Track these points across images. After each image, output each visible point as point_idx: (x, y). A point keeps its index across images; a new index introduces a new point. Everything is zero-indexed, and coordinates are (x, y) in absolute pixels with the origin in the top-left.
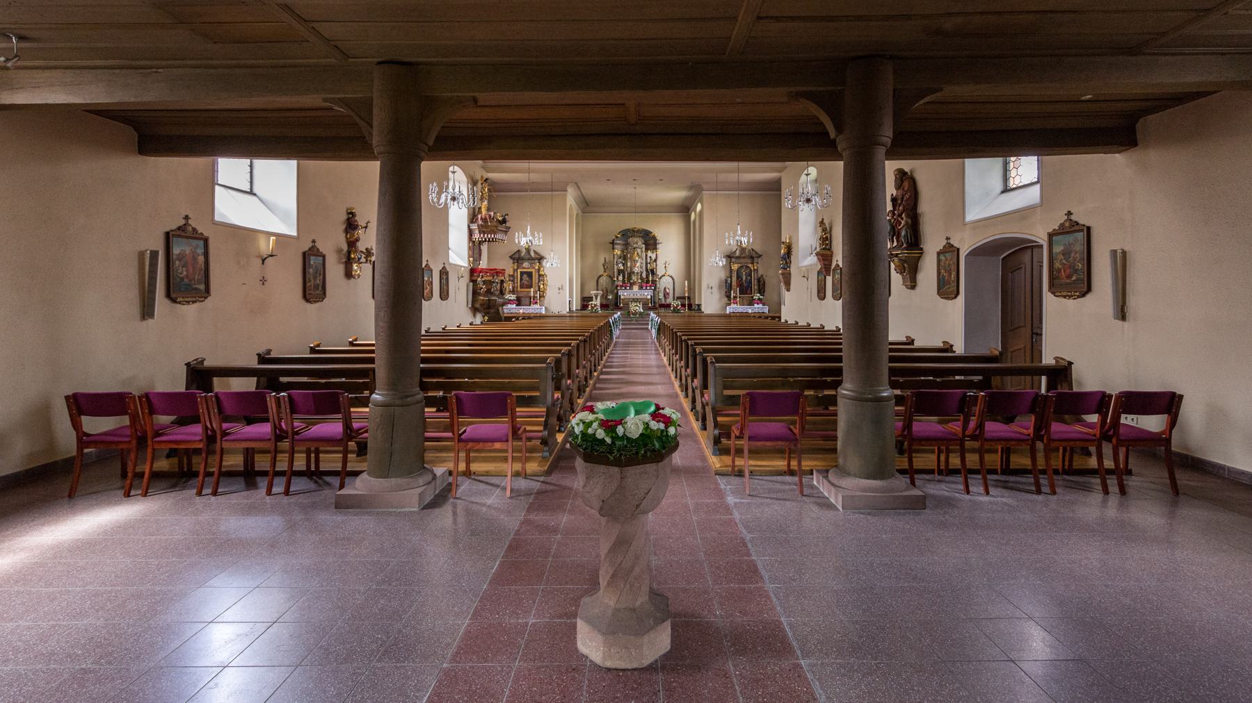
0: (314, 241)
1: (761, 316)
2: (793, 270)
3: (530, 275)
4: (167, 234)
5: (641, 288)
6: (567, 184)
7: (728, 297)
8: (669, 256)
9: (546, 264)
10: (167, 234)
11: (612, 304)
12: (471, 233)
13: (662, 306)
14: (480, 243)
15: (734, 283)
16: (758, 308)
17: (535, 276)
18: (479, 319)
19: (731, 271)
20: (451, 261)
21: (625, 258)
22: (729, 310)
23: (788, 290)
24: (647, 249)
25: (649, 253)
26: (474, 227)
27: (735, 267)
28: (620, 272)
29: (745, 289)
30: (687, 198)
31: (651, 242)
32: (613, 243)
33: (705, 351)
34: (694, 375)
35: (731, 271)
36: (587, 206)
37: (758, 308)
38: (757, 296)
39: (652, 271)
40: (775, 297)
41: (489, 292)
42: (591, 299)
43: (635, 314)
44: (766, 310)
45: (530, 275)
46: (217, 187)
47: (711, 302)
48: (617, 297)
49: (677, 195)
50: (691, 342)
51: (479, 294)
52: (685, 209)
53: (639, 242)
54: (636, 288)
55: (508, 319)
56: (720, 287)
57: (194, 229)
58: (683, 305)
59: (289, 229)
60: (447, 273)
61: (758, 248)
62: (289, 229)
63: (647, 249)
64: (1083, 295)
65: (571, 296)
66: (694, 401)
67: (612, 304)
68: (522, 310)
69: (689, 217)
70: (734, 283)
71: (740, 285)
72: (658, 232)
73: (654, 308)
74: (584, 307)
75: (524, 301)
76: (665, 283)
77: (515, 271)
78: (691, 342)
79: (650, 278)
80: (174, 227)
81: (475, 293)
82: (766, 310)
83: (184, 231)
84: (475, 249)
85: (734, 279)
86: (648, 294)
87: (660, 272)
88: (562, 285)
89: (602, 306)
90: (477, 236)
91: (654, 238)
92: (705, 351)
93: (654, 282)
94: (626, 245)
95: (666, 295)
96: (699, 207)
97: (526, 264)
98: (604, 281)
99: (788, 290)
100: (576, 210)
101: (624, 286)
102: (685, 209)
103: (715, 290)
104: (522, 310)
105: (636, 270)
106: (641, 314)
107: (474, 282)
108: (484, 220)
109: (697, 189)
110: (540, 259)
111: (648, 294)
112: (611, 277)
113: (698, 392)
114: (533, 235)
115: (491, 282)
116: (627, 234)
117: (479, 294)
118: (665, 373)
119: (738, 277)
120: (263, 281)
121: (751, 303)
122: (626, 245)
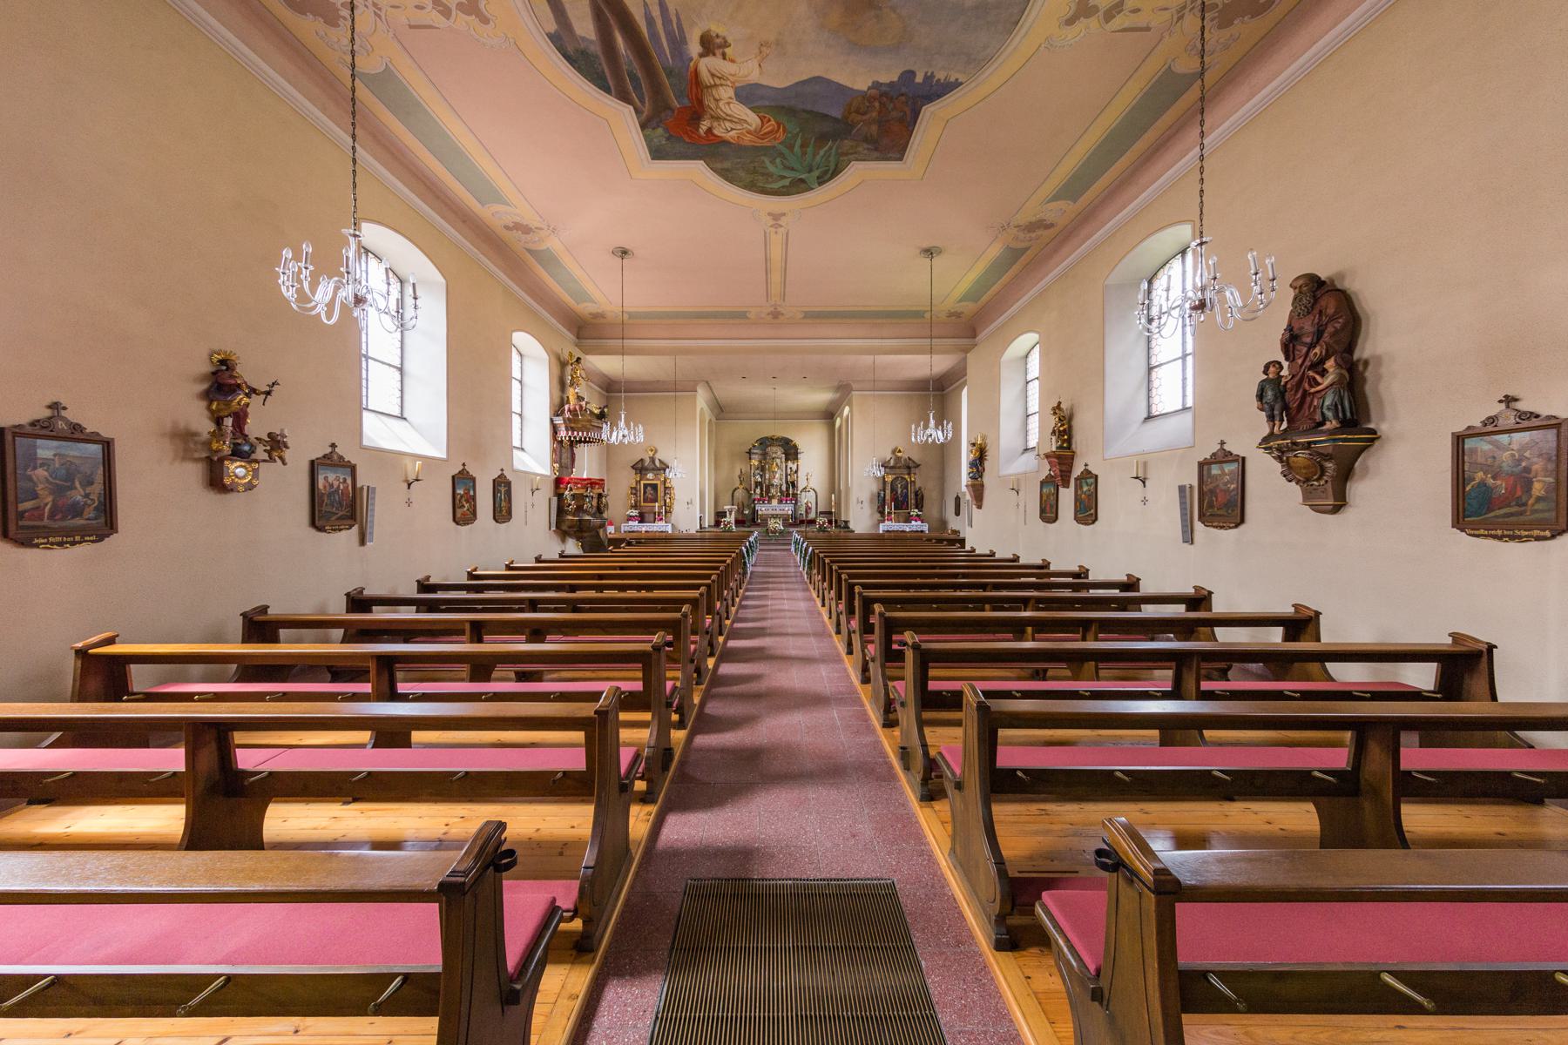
0: (333, 446)
1: (918, 536)
2: (987, 479)
3: (655, 487)
4: (312, 462)
5: (780, 502)
6: (696, 383)
7: (882, 513)
8: (811, 469)
9: (670, 474)
10: (312, 462)
11: (749, 519)
12: (555, 429)
13: (802, 522)
14: (572, 443)
15: (888, 497)
16: (915, 525)
17: (661, 489)
18: (572, 547)
19: (884, 482)
20: (517, 465)
21: (763, 469)
22: (882, 528)
23: (979, 507)
24: (787, 460)
25: (790, 464)
26: (559, 421)
27: (889, 479)
28: (758, 484)
29: (901, 503)
30: (832, 402)
31: (791, 452)
32: (749, 453)
33: (851, 576)
34: (839, 597)
35: (884, 482)
36: (722, 412)
37: (915, 525)
38: (915, 512)
39: (793, 484)
40: (935, 513)
41: (580, 509)
42: (723, 514)
43: (774, 532)
44: (925, 528)
45: (655, 487)
46: (365, 414)
47: (861, 519)
48: (754, 512)
49: (820, 397)
50: (840, 564)
51: (567, 513)
52: (829, 415)
53: (777, 452)
54: (775, 502)
55: (616, 542)
56: (871, 501)
57: (341, 457)
58: (830, 522)
59: (436, 449)
60: (508, 484)
61: (915, 458)
62: (436, 449)
63: (787, 460)
64: (100, 538)
65: (702, 510)
66: (838, 624)
67: (749, 519)
68: (644, 527)
69: (833, 424)
70: (888, 497)
71: (894, 499)
72: (800, 440)
73: (793, 525)
74: (717, 524)
75: (649, 517)
76: (806, 498)
77: (638, 482)
78: (840, 564)
79: (790, 492)
80: (320, 455)
81: (561, 511)
82: (925, 528)
83: (331, 460)
84: (564, 451)
85: (888, 492)
86: (788, 509)
87: (801, 485)
88: (691, 505)
89: (738, 522)
90: (563, 433)
91: (795, 447)
92: (851, 576)
93: (795, 495)
94: (764, 455)
95: (808, 509)
96: (847, 410)
97: (650, 476)
98: (740, 494)
99: (979, 507)
100: (708, 415)
101: (762, 500)
102: (829, 415)
103: (866, 505)
104: (644, 527)
105: (776, 481)
106: (781, 532)
107: (560, 496)
108: (573, 412)
109: (844, 390)
110: (664, 467)
111: (788, 509)
112: (748, 490)
113: (843, 618)
114: (628, 425)
115: (583, 497)
116: (765, 443)
117: (567, 513)
118: (811, 599)
119: (893, 490)
120: (409, 503)
121: (908, 519)
122: (764, 455)
